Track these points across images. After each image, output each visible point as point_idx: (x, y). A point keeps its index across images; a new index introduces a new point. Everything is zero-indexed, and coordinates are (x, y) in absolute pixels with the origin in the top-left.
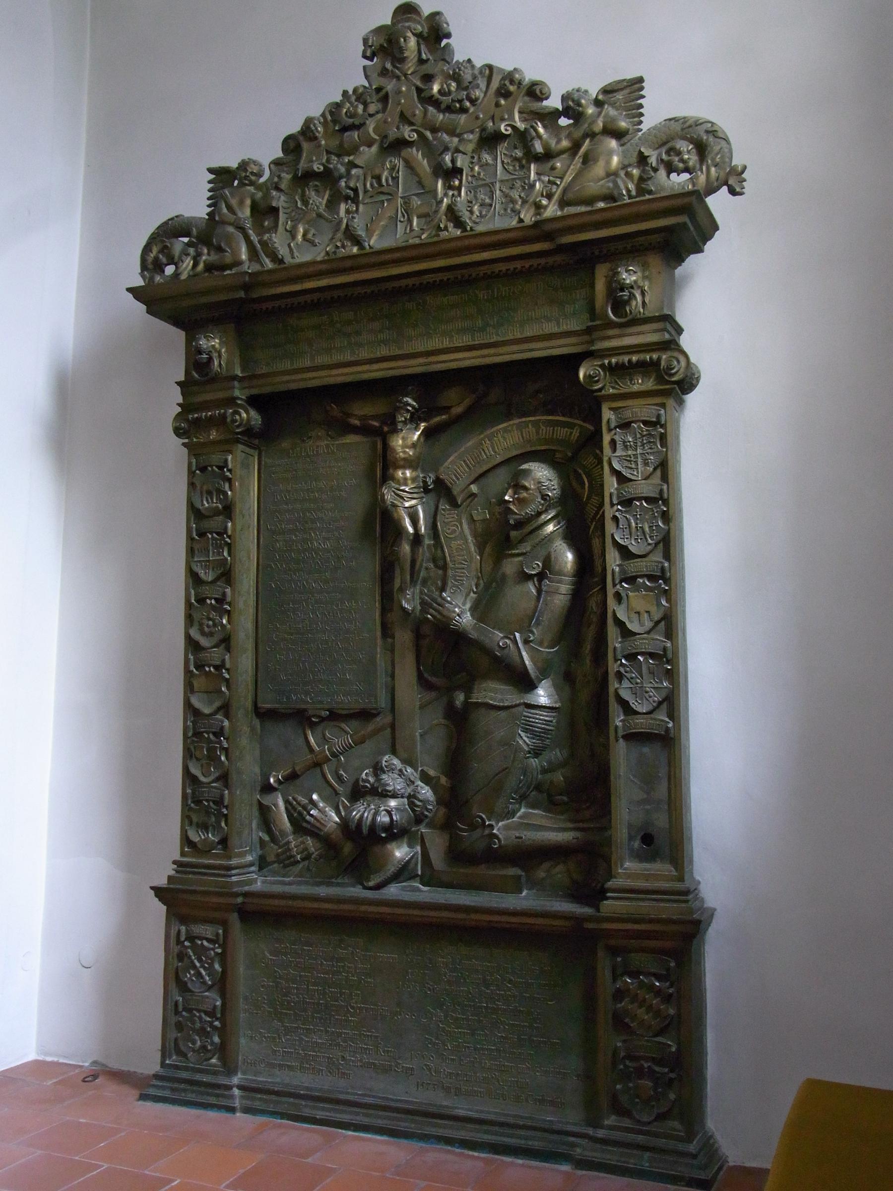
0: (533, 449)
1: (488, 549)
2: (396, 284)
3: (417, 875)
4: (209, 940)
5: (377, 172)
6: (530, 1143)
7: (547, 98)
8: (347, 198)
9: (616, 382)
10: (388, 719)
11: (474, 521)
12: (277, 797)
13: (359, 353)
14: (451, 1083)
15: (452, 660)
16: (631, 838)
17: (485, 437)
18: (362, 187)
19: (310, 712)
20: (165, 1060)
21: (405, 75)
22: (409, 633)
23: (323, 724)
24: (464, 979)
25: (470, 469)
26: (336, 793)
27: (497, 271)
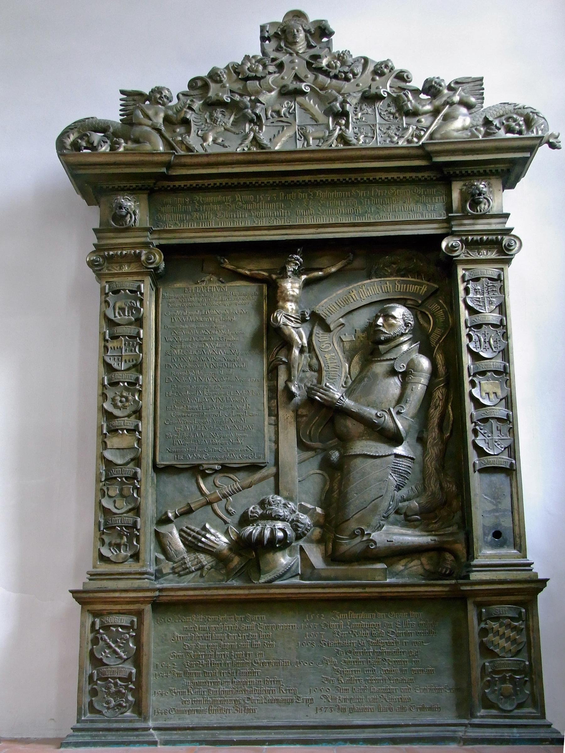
1: (356, 359)
2: (295, 179)
4: (122, 627)
7: (410, 82)
8: (251, 121)
9: (468, 253)
10: (273, 470)
11: (342, 341)
12: (172, 528)
14: (346, 705)
15: (329, 427)
16: (485, 534)
19: (205, 466)
20: (81, 717)
21: (297, 53)
22: (291, 412)
26: (226, 522)
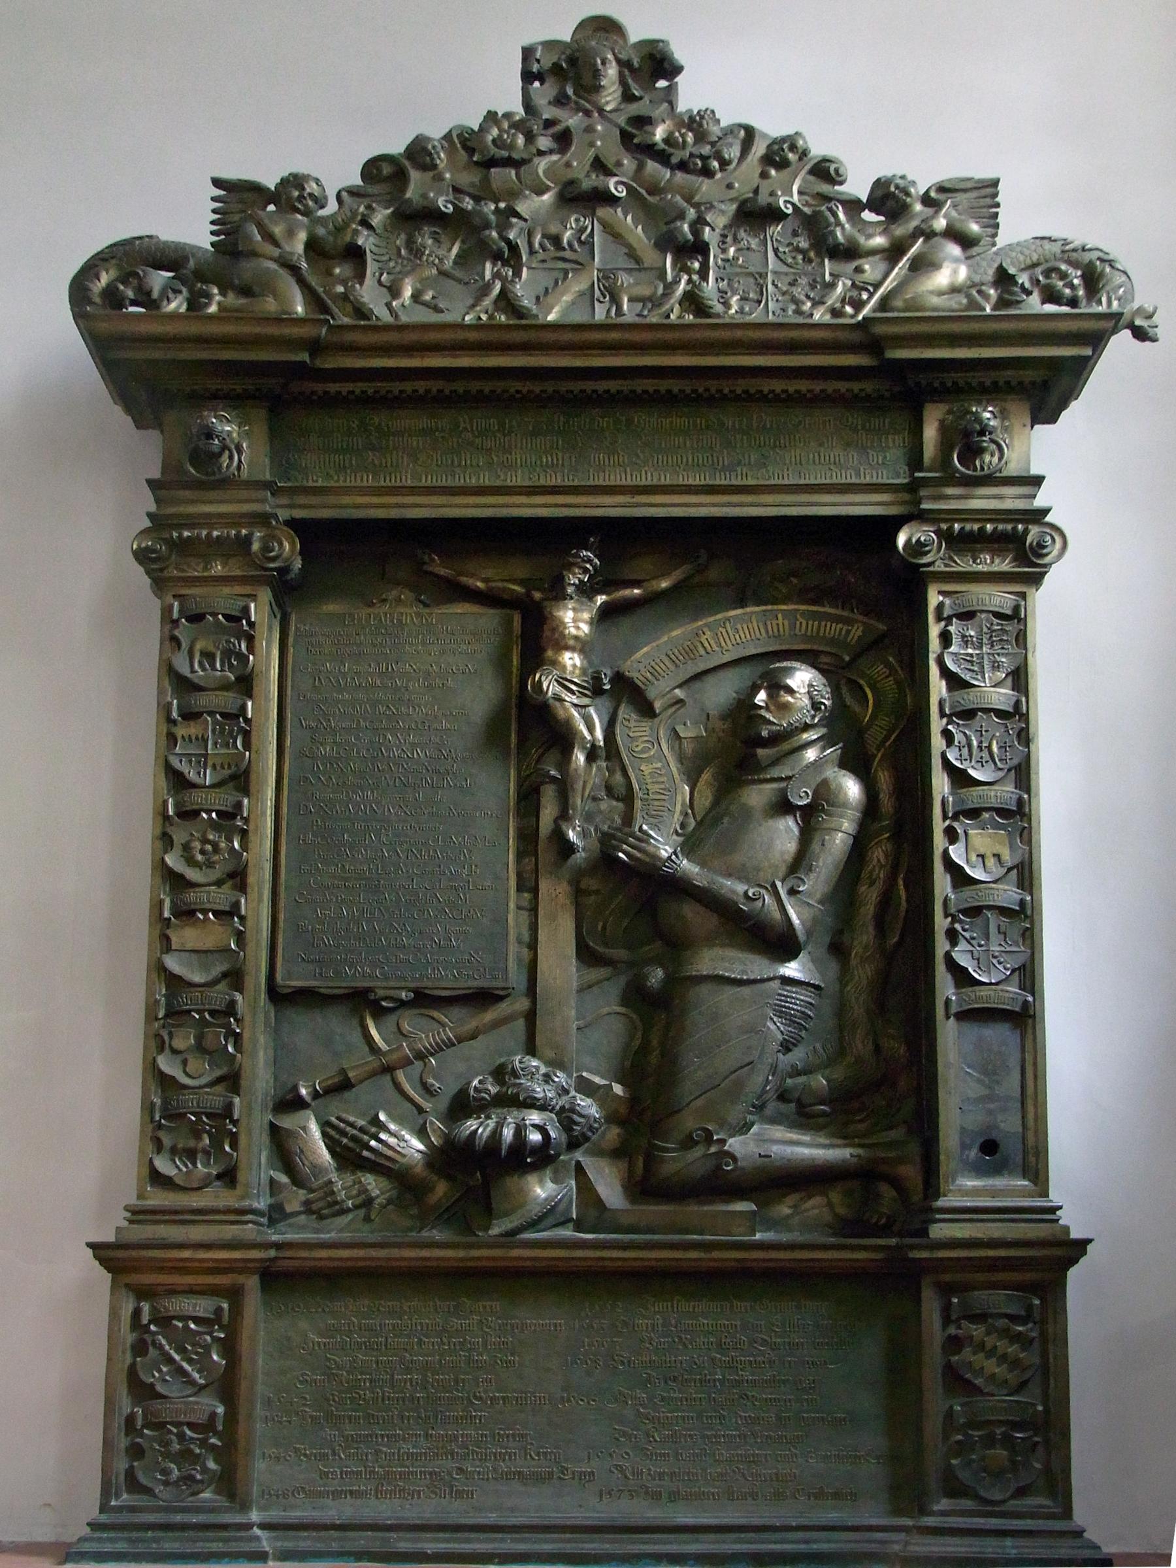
0: (784, 647)
1: (706, 776)
3: (570, 1220)
4: (196, 1320)
5: (553, 229)
6: (815, 1546)
7: (841, 183)
8: (497, 257)
10: (523, 1004)
12: (308, 1119)
13: (519, 477)
15: (645, 921)
16: (964, 1146)
17: (706, 625)
18: (526, 246)
19: (381, 993)
22: (565, 884)
23: (398, 1013)
24: (685, 1345)
25: (677, 666)
26: (420, 1110)
27: (766, 390)
